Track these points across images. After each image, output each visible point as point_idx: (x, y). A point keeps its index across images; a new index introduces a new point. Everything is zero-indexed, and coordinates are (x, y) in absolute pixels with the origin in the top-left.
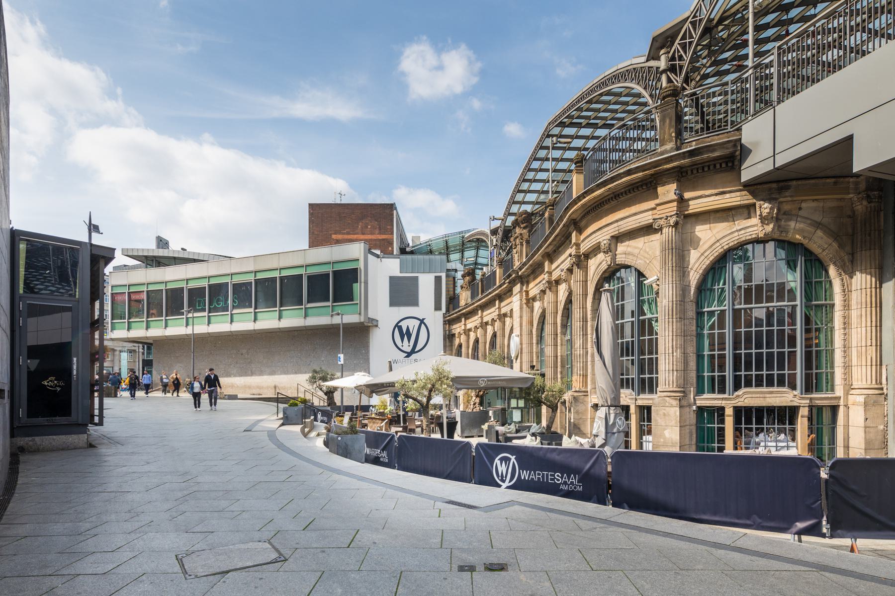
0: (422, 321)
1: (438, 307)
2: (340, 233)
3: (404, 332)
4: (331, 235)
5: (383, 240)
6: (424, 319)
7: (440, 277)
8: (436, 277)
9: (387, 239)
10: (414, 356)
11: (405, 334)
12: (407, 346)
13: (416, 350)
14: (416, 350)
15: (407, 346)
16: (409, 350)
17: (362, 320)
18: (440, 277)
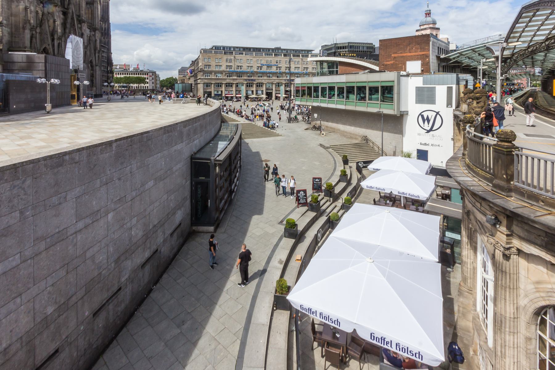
0: (438, 113)
1: (449, 104)
2: (396, 53)
3: (425, 119)
4: (391, 55)
5: (423, 55)
7: (452, 87)
8: (448, 87)
9: (425, 54)
10: (431, 132)
12: (427, 127)
13: (433, 130)
14: (433, 130)
15: (427, 127)
16: (428, 129)
17: (396, 114)
18: (452, 87)
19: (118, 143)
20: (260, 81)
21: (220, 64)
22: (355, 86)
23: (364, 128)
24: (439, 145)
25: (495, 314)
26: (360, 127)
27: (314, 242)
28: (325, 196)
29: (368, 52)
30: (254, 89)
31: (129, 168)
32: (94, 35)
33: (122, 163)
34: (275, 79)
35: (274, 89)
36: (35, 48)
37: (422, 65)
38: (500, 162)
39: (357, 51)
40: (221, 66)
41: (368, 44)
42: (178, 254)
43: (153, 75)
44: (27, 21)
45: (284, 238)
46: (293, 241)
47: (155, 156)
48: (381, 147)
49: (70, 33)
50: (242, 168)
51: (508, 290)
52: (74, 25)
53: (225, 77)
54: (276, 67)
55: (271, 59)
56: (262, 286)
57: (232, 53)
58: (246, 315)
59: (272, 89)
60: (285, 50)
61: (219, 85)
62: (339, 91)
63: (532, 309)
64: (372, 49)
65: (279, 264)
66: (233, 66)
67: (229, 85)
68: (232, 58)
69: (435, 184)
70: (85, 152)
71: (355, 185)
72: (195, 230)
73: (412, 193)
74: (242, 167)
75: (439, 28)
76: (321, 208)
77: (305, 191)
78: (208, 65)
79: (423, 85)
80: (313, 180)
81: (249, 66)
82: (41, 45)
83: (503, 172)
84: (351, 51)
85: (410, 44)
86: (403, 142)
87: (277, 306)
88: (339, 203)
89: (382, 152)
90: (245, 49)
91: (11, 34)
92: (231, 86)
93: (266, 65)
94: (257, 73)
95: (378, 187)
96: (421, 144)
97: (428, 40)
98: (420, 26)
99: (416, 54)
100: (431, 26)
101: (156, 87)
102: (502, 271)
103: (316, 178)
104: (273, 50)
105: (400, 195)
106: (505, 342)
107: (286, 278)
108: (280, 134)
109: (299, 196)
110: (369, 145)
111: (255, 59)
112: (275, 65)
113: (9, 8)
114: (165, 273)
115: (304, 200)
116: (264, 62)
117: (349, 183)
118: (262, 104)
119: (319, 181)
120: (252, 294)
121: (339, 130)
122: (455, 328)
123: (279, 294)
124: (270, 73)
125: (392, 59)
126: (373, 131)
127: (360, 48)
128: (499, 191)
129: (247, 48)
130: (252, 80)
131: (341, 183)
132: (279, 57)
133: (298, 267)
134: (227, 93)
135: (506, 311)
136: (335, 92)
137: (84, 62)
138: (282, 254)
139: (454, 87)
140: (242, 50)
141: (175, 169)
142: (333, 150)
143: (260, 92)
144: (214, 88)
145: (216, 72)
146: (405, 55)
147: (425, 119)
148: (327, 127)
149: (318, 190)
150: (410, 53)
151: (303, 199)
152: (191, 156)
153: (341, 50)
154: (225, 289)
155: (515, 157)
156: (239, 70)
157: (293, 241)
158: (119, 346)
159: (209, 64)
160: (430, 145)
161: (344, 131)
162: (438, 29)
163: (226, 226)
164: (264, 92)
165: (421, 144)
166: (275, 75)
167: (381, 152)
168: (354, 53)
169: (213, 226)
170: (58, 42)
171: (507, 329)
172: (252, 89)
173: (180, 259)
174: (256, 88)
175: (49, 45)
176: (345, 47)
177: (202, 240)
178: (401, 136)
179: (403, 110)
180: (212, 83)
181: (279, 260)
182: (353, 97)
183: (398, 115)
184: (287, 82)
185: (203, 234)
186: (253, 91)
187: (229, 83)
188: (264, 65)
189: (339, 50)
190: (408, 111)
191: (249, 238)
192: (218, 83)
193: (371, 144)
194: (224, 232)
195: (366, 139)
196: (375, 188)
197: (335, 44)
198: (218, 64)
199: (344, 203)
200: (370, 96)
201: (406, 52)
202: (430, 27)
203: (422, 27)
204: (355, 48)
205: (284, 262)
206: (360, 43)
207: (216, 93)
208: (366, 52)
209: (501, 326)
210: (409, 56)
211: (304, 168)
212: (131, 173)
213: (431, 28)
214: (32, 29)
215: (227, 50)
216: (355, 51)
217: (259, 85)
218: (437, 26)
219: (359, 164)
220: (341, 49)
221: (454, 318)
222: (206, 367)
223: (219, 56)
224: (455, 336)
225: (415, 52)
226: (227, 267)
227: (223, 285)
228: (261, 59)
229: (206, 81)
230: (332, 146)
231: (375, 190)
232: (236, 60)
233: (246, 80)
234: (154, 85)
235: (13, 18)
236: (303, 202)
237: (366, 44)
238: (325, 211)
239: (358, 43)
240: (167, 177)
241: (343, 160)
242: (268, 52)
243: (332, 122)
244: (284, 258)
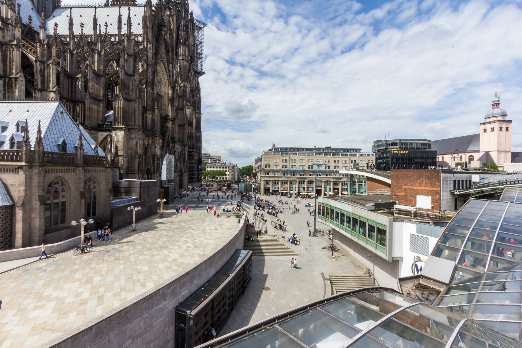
2: (407, 185)
5: (433, 190)
19: (98, 325)
20: (310, 179)
21: (278, 164)
29: (422, 148)
30: (305, 186)
31: (107, 339)
32: (184, 150)
33: (101, 337)
34: (324, 177)
35: (323, 187)
36: (141, 170)
37: (433, 201)
39: (410, 148)
40: (278, 165)
41: (422, 140)
43: (232, 168)
44: (136, 153)
47: (134, 322)
49: (166, 153)
52: (169, 146)
53: (281, 176)
54: (325, 166)
55: (321, 159)
57: (287, 154)
59: (322, 187)
60: (334, 149)
61: (276, 182)
64: (426, 145)
66: (288, 165)
67: (284, 182)
68: (288, 158)
70: (69, 342)
78: (268, 165)
81: (301, 166)
82: (145, 166)
84: (402, 148)
85: (420, 178)
90: (298, 149)
91: (128, 162)
92: (286, 183)
93: (316, 164)
94: (308, 171)
97: (439, 176)
98: (486, 118)
99: (426, 188)
100: (500, 118)
101: (234, 178)
104: (323, 149)
111: (306, 159)
112: (324, 164)
113: (128, 144)
116: (314, 162)
124: (319, 172)
125: (403, 190)
127: (412, 145)
129: (301, 149)
130: (304, 178)
132: (328, 156)
134: (282, 189)
137: (175, 172)
140: (296, 150)
141: (155, 324)
143: (310, 189)
144: (272, 184)
145: (274, 171)
146: (415, 188)
147: (419, 269)
148: (342, 248)
150: (420, 186)
152: (176, 307)
153: (392, 147)
156: (293, 169)
159: (269, 164)
161: (354, 257)
162: (510, 121)
164: (314, 189)
166: (324, 173)
168: (405, 150)
170: (157, 161)
172: (303, 186)
174: (307, 185)
175: (151, 165)
176: (397, 144)
179: (396, 256)
180: (270, 181)
183: (389, 261)
184: (335, 180)
186: (304, 188)
187: (284, 181)
188: (314, 164)
189: (390, 147)
192: (276, 181)
197: (386, 141)
198: (276, 164)
201: (417, 185)
202: (498, 120)
203: (488, 120)
204: (407, 145)
206: (412, 140)
207: (273, 189)
208: (419, 148)
210: (419, 190)
212: (109, 341)
213: (499, 121)
214: (140, 157)
215: (284, 151)
216: (407, 148)
217: (310, 183)
218: (507, 118)
220: (392, 145)
223: (277, 157)
225: (425, 187)
228: (312, 158)
229: (266, 179)
232: (290, 160)
233: (298, 178)
234: (233, 176)
235: (130, 151)
237: (419, 140)
239: (410, 140)
240: (146, 333)
242: (318, 151)
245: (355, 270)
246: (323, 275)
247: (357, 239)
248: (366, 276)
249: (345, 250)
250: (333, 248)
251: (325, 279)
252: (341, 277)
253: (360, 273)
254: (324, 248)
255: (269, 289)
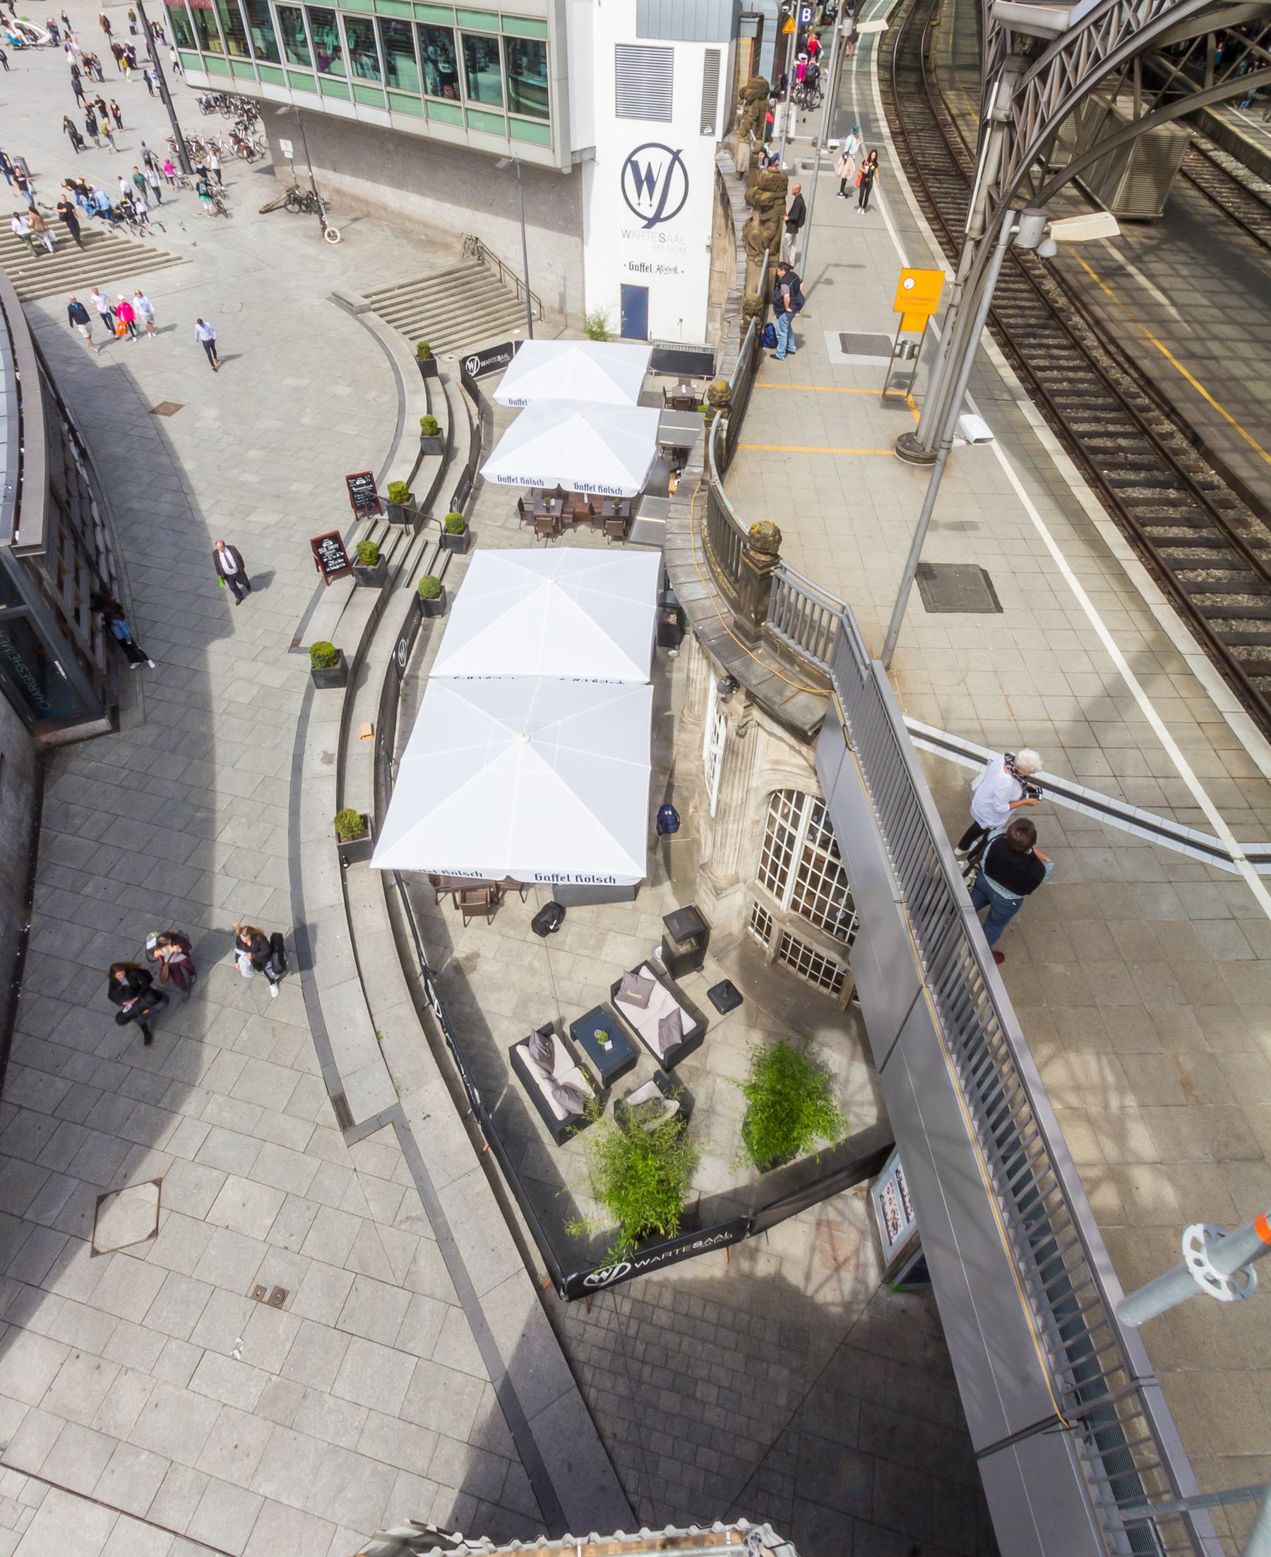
1: (707, 121)
3: (643, 178)
6: (679, 151)
10: (658, 226)
11: (645, 181)
13: (662, 217)
14: (662, 217)
16: (650, 213)
17: (559, 165)
22: (413, 20)
23: (467, 207)
24: (675, 269)
25: (718, 802)
26: (454, 199)
27: (394, 674)
28: (391, 521)
38: (749, 588)
42: (39, 826)
45: (317, 692)
46: (342, 691)
48: (523, 279)
50: (91, 457)
51: (738, 774)
56: (303, 829)
58: (289, 903)
62: (354, 36)
63: (764, 792)
65: (326, 766)
69: (657, 443)
71: (467, 462)
72: (50, 741)
73: (605, 484)
74: (89, 452)
75: (640, 403)
76: (390, 564)
77: (335, 537)
79: (638, 36)
80: (349, 484)
83: (752, 608)
86: (583, 262)
87: (350, 859)
88: (432, 532)
89: (529, 296)
95: (527, 475)
96: (632, 267)
102: (733, 752)
103: (355, 477)
105: (579, 491)
106: (727, 832)
107: (349, 804)
108: (173, 255)
109: (323, 555)
110: (488, 270)
114: (36, 885)
115: (340, 561)
117: (448, 452)
118: (19, 32)
119: (367, 484)
120: (287, 856)
121: (385, 208)
122: (671, 775)
123: (348, 840)
126: (495, 218)
128: (742, 638)
131: (427, 459)
133: (370, 754)
135: (731, 799)
136: (337, 37)
138: (324, 738)
139: (724, 48)
142: (382, 321)
148: (339, 192)
149: (370, 508)
151: (335, 559)
154: (218, 868)
155: (774, 581)
157: (342, 691)
158: (27, 1070)
160: (654, 268)
161: (401, 215)
163: (140, 699)
165: (632, 267)
167: (524, 295)
169: (103, 717)
171: (731, 818)
173: (56, 837)
177: (90, 765)
178: (578, 239)
181: (322, 755)
182: (410, 68)
185: (81, 745)
190: (593, 148)
191: (225, 717)
193: (495, 269)
194: (146, 722)
195: (476, 249)
196: (519, 480)
199: (446, 531)
200: (471, 75)
205: (336, 757)
209: (724, 816)
211: (306, 420)
219: (468, 363)
221: (672, 754)
222: (246, 1021)
224: (670, 787)
226: (199, 814)
227: (209, 860)
230: (376, 294)
231: (520, 484)
236: (338, 567)
238: (400, 569)
241: (419, 364)
243: (353, 175)
244: (332, 746)
245: (427, 255)
246: (338, 299)
247: (423, 122)
248: (471, 263)
249: (355, 198)
250: (306, 203)
251: (356, 311)
252: (397, 292)
253: (448, 261)
254: (268, 210)
255: (178, 407)
